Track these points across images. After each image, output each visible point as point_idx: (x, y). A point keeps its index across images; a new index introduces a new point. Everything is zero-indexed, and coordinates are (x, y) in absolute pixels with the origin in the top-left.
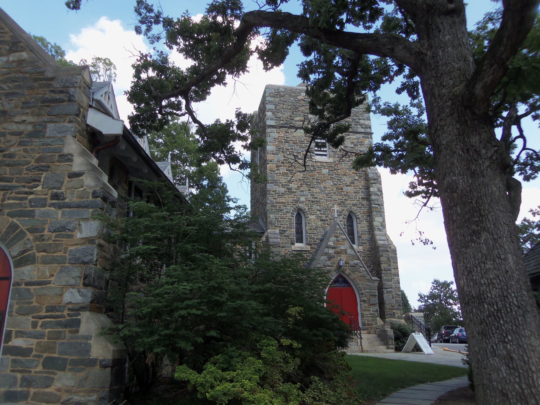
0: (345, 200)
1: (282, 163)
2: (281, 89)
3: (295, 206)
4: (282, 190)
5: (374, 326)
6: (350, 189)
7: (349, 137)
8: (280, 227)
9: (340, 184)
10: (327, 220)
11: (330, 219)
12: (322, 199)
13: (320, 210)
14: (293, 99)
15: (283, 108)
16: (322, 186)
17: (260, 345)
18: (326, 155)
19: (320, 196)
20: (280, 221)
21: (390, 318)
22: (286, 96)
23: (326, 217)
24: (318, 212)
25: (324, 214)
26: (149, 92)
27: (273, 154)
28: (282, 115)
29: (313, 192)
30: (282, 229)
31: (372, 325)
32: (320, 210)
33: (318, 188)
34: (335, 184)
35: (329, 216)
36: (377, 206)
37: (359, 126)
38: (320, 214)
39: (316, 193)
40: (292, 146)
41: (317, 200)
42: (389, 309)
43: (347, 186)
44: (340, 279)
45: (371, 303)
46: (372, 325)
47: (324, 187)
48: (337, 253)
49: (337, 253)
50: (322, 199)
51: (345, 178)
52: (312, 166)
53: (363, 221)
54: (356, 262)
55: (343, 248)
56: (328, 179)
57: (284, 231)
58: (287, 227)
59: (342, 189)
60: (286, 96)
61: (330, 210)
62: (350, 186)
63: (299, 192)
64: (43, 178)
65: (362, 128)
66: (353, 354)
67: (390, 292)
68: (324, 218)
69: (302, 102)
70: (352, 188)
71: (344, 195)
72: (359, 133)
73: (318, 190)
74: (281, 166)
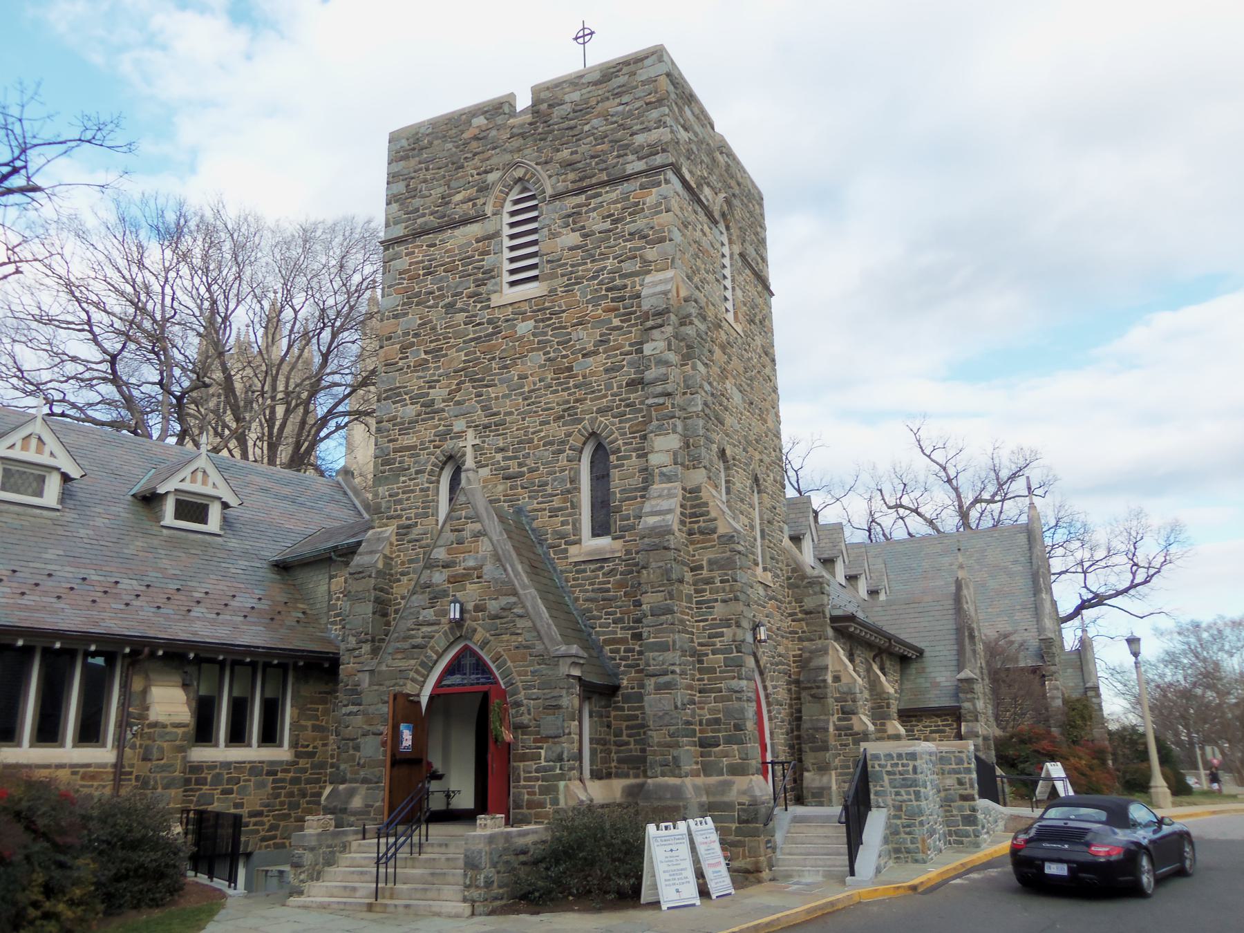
0: (577, 401)
1: (416, 335)
2: (422, 130)
3: (438, 451)
4: (411, 410)
5: (549, 808)
6: (596, 363)
7: (600, 199)
8: (400, 517)
9: (564, 357)
10: (521, 475)
11: (531, 471)
12: (511, 413)
13: (502, 450)
14: (450, 145)
15: (425, 181)
16: (514, 373)
17: (72, 903)
18: (535, 278)
19: (507, 405)
20: (400, 502)
21: (663, 775)
22: (436, 142)
23: (520, 465)
24: (499, 456)
25: (516, 458)
26: (212, 243)
27: (396, 317)
28: (422, 201)
29: (490, 399)
30: (404, 522)
31: (542, 805)
32: (502, 450)
33: (502, 381)
34: (549, 360)
35: (528, 462)
36: (661, 400)
37: (631, 157)
38: (505, 459)
39: (497, 398)
40: (441, 280)
41: (497, 419)
42: (659, 744)
43: (584, 356)
44: (468, 661)
45: (544, 733)
46: (542, 805)
47: (520, 378)
48: (455, 580)
49: (455, 580)
50: (511, 413)
51: (581, 333)
52: (490, 322)
53: (629, 457)
54: (504, 601)
55: (471, 563)
56: (533, 350)
57: (409, 527)
58: (417, 516)
59: (570, 369)
60: (436, 142)
61: (531, 441)
62: (596, 353)
63: (451, 409)
64: (469, 452)
65: (640, 159)
66: (1071, 824)
67: (668, 686)
68: (514, 468)
69: (474, 144)
70: (602, 357)
71: (576, 386)
72: (627, 178)
73: (503, 389)
74: (412, 344)
